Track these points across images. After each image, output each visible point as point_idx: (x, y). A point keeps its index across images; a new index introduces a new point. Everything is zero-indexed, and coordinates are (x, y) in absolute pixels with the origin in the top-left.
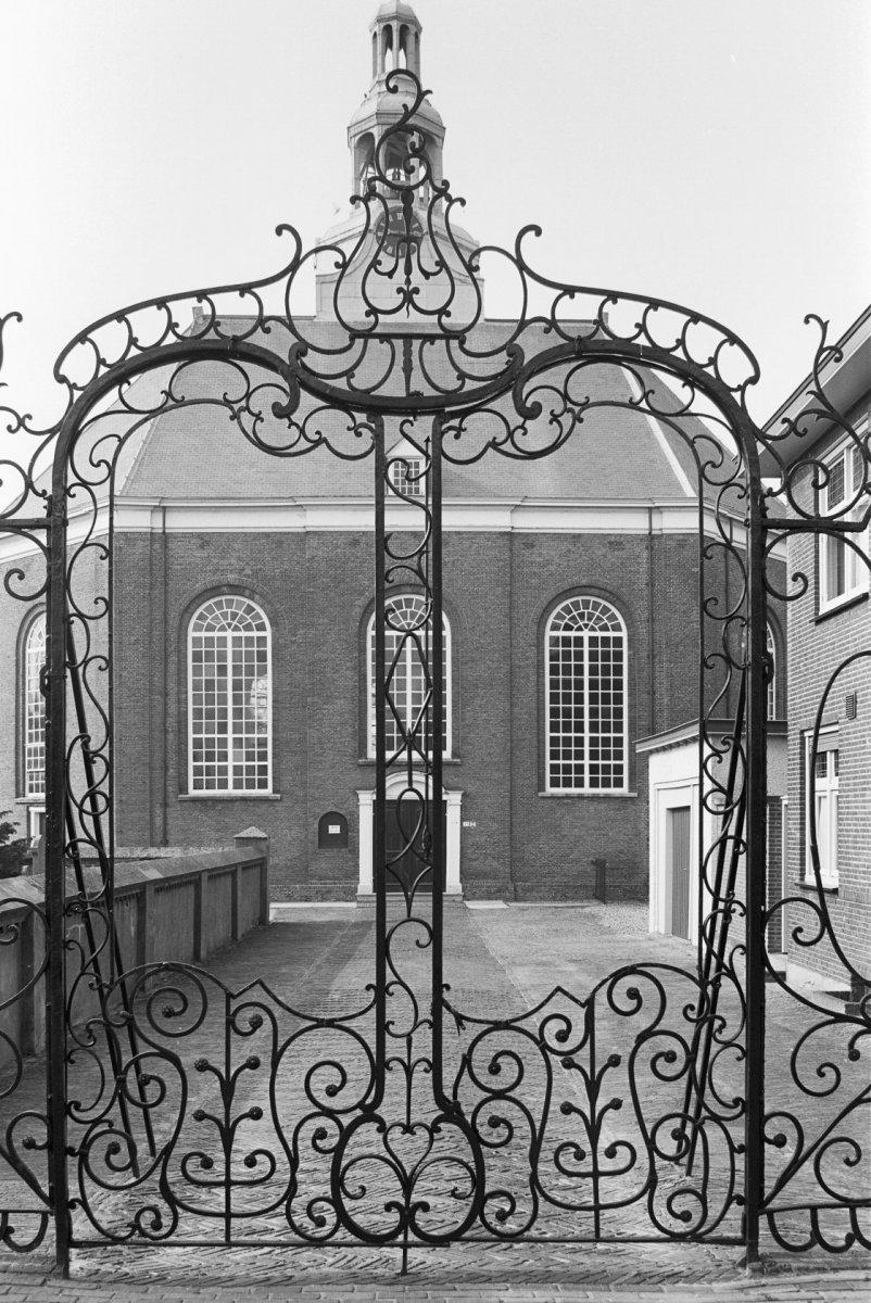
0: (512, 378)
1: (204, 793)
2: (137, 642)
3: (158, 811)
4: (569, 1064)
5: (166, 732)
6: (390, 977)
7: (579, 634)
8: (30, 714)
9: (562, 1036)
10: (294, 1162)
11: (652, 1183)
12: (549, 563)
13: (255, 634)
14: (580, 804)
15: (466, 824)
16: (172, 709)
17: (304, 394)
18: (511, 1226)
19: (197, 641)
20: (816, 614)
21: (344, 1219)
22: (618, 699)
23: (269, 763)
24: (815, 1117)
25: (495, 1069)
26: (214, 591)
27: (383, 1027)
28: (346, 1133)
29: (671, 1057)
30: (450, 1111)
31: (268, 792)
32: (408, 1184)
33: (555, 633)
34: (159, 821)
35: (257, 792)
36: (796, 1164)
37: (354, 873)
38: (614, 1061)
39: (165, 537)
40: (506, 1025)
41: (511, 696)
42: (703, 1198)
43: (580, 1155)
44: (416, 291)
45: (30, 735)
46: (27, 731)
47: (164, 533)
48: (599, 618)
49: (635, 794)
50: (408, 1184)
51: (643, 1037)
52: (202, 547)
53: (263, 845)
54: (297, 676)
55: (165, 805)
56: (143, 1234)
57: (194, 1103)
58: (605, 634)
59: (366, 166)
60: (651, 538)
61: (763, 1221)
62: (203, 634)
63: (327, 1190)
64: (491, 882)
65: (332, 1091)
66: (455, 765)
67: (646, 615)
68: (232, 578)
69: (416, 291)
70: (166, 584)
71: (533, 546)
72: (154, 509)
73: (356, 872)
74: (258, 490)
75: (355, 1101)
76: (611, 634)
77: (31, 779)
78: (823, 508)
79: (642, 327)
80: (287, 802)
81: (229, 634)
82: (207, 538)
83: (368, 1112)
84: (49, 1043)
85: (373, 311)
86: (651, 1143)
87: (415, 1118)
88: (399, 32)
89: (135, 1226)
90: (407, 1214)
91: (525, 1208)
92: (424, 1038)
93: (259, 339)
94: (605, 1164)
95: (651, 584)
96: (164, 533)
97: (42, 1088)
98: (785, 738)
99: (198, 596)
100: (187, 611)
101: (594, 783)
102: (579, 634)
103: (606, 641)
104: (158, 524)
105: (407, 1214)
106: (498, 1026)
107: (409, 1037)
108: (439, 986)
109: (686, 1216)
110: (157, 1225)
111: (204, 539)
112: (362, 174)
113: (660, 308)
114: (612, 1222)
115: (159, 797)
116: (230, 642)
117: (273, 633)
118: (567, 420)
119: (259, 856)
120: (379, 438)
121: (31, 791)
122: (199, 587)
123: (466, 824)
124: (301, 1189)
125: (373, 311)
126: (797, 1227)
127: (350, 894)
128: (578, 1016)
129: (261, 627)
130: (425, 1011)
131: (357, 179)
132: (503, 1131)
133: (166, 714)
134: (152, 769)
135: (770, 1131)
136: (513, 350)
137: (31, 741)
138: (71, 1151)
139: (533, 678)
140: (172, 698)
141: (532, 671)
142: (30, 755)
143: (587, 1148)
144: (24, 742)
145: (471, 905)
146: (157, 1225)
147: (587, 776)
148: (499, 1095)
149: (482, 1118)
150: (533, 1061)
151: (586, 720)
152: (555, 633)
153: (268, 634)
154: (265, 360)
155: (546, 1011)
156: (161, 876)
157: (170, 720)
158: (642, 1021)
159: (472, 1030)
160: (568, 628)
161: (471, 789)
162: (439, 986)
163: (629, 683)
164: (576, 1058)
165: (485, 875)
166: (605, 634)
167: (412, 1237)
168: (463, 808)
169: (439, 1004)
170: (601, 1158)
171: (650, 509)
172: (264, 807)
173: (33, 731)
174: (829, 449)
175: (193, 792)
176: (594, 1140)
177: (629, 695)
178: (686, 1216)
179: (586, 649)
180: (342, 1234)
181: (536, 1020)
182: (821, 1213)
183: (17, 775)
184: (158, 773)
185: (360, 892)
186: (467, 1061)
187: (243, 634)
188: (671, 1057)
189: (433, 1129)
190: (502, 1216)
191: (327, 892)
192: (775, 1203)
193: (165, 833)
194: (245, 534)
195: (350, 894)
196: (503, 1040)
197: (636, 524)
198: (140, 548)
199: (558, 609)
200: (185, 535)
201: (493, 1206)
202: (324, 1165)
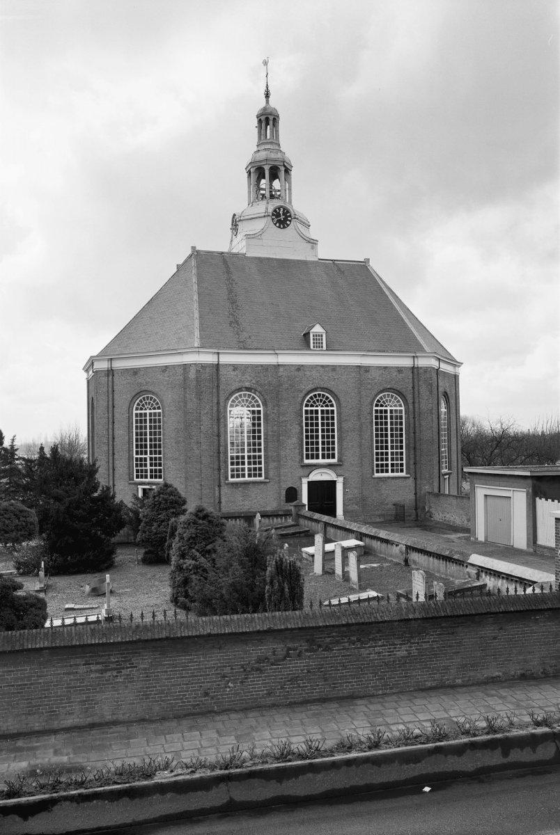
7: (316, 408)
12: (374, 379)
14: (389, 481)
26: (239, 390)
31: (262, 478)
33: (307, 408)
35: (258, 479)
48: (251, 402)
49: (408, 476)
52: (234, 370)
58: (155, 411)
60: (414, 369)
62: (309, 408)
66: (340, 465)
67: (412, 401)
68: (247, 384)
71: (368, 371)
76: (330, 408)
81: (148, 411)
84: (475, 587)
96: (218, 364)
100: (228, 399)
101: (392, 471)
102: (316, 408)
103: (328, 411)
111: (235, 367)
113: (175, 270)
117: (263, 409)
122: (233, 388)
129: (259, 406)
147: (390, 468)
151: (389, 444)
152: (307, 408)
157: (221, 448)
160: (312, 406)
166: (155, 411)
168: (344, 484)
175: (231, 480)
179: (320, 415)
197: (406, 362)
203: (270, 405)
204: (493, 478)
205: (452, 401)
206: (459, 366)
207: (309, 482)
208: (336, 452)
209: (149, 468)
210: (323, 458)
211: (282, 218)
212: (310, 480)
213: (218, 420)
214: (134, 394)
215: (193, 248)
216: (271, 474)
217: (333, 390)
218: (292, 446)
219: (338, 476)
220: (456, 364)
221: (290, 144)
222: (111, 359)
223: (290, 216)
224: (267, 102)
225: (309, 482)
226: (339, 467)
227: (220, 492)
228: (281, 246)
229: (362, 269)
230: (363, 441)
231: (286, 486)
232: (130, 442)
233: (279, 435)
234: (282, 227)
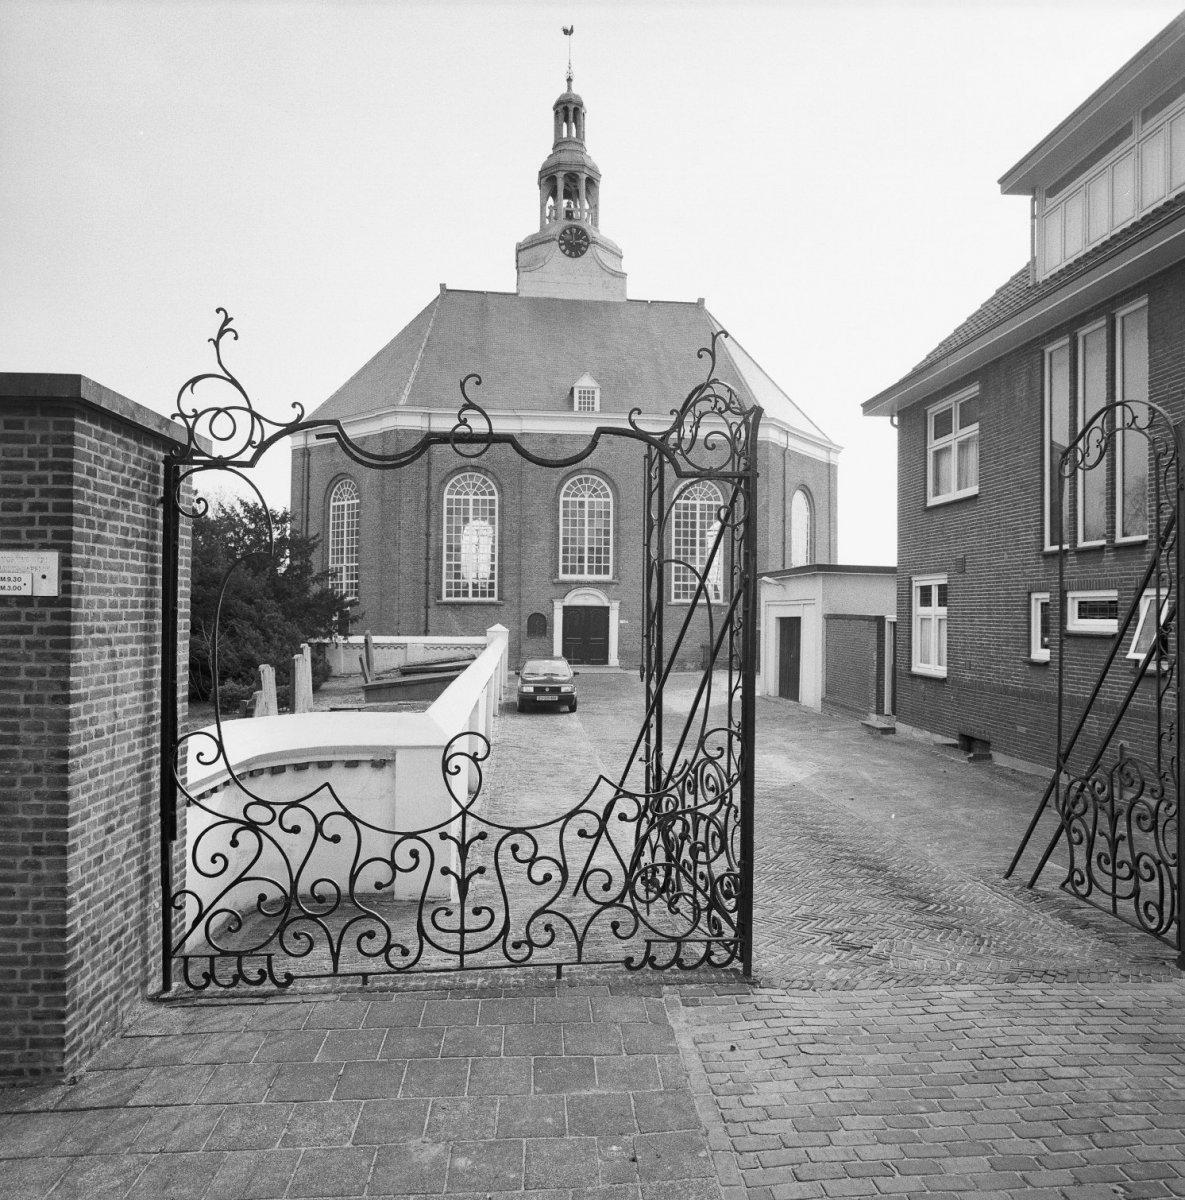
1: (453, 599)
2: (410, 501)
5: (427, 559)
13: (488, 497)
16: (433, 544)
19: (450, 501)
31: (494, 599)
35: (487, 599)
54: (514, 525)
55: (427, 607)
62: (454, 497)
88: (568, 110)
99: (452, 472)
100: (444, 482)
102: (582, 499)
116: (471, 503)
129: (492, 493)
152: (450, 497)
153: (496, 497)
161: (625, 599)
175: (445, 599)
187: (480, 497)
199: (575, 478)
203: (508, 491)
205: (821, 502)
206: (838, 452)
207: (565, 608)
209: (344, 581)
210: (590, 572)
211: (576, 242)
212: (567, 604)
213: (428, 512)
214: (329, 479)
215: (443, 286)
216: (507, 593)
217: (608, 472)
220: (838, 450)
221: (598, 147)
224: (569, 88)
225: (565, 608)
228: (563, 279)
231: (527, 612)
233: (521, 536)
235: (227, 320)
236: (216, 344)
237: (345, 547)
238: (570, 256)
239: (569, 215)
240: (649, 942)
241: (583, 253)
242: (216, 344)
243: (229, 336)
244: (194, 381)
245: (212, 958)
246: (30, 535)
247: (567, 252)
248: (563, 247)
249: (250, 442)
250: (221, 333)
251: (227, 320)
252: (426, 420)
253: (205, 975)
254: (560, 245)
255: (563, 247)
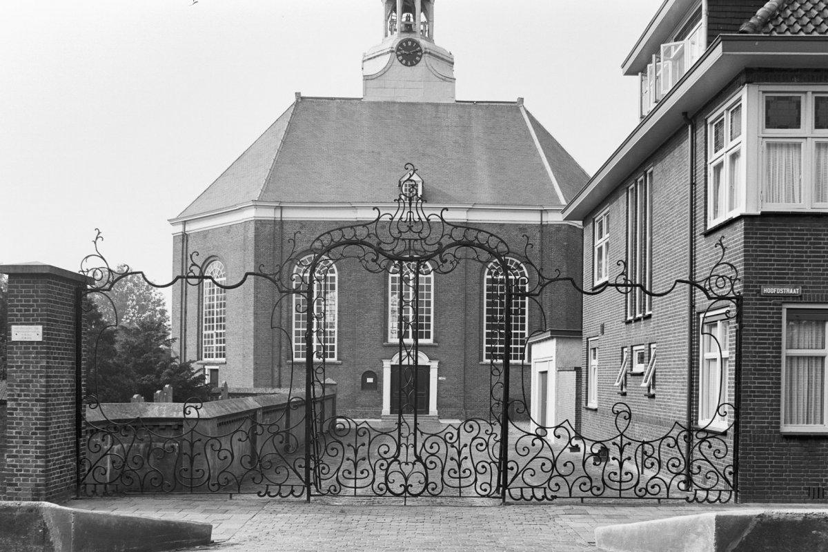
0: (440, 251)
3: (276, 369)
4: (453, 446)
6: (402, 420)
8: (206, 315)
9: (451, 438)
10: (374, 473)
11: (476, 480)
15: (440, 378)
16: (285, 315)
17: (380, 255)
18: (436, 492)
20: (593, 286)
21: (388, 489)
22: (523, 312)
23: (336, 344)
24: (522, 462)
25: (431, 447)
27: (400, 435)
28: (389, 465)
29: (481, 445)
30: (419, 459)
31: (335, 360)
32: (406, 479)
34: (276, 375)
36: (516, 475)
37: (380, 404)
38: (465, 445)
39: (282, 223)
40: (435, 435)
41: (465, 310)
42: (490, 485)
43: (455, 472)
44: (412, 226)
45: (206, 327)
46: (204, 325)
47: (281, 221)
50: (406, 479)
51: (473, 439)
53: (334, 388)
55: (280, 366)
56: (331, 493)
57: (347, 455)
59: (391, 12)
60: (542, 227)
61: (507, 491)
63: (383, 481)
64: (453, 410)
65: (385, 453)
66: (435, 346)
69: (412, 226)
70: (282, 248)
72: (276, 208)
73: (381, 403)
74: (332, 197)
75: (392, 456)
77: (206, 350)
78: (711, 150)
79: (476, 238)
80: (345, 365)
82: (304, 224)
83: (396, 458)
85: (400, 232)
86: (475, 469)
87: (409, 461)
89: (329, 491)
90: (406, 489)
91: (440, 486)
92: (412, 437)
93: (367, 240)
94: (462, 475)
95: (541, 251)
96: (281, 221)
97: (304, 452)
98: (581, 338)
104: (278, 215)
105: (406, 489)
106: (432, 435)
107: (407, 437)
108: (416, 424)
109: (485, 490)
110: (335, 490)
111: (303, 224)
112: (389, 17)
114: (465, 491)
115: (276, 361)
118: (455, 264)
119: (332, 393)
120: (401, 268)
121: (206, 357)
123: (440, 378)
124: (376, 480)
125: (400, 232)
126: (516, 493)
127: (378, 415)
128: (455, 432)
130: (412, 431)
131: (386, 21)
132: (434, 465)
133: (281, 317)
134: (273, 347)
135: (510, 465)
136: (440, 244)
137: (206, 330)
138: (311, 469)
139: (478, 301)
140: (284, 309)
141: (477, 297)
142: (205, 338)
143: (457, 469)
144: (202, 331)
145: (441, 421)
146: (335, 490)
148: (433, 455)
149: (428, 462)
150: (443, 446)
154: (370, 246)
155: (446, 431)
156: (260, 406)
157: (283, 321)
158: (474, 433)
159: (425, 436)
161: (443, 359)
162: (416, 424)
163: (529, 304)
164: (455, 445)
165: (450, 406)
167: (408, 495)
169: (416, 429)
170: (462, 473)
171: (541, 211)
172: (333, 367)
173: (208, 324)
174: (716, 109)
176: (459, 469)
177: (529, 310)
178: (485, 490)
180: (388, 494)
181: (444, 433)
182: (523, 489)
183: (198, 348)
184: (276, 349)
185: (383, 414)
186: (424, 445)
188: (481, 445)
189: (414, 464)
190: (433, 489)
191: (366, 414)
192: (511, 486)
193: (280, 381)
194: (325, 221)
195: (378, 415)
196: (434, 439)
197: (534, 218)
198: (268, 228)
200: (292, 222)
201: (431, 486)
202: (383, 473)
204: (814, 165)
208: (432, 330)
212: (394, 363)
218: (372, 321)
219: (431, 359)
222: (185, 221)
223: (421, 51)
226: (433, 349)
227: (280, 373)
228: (412, 86)
229: (514, 108)
230: (468, 318)
232: (482, 292)
234: (409, 64)
235: (99, 233)
236: (95, 243)
237: (215, 317)
238: (406, 65)
239: (408, 28)
240: (268, 485)
241: (417, 62)
242: (95, 243)
243: (100, 239)
244: (87, 257)
245: (95, 485)
246: (33, 320)
247: (404, 62)
248: (401, 58)
249: (108, 281)
250: (97, 238)
251: (99, 233)
252: (278, 212)
253: (92, 491)
254: (398, 56)
255: (401, 58)
